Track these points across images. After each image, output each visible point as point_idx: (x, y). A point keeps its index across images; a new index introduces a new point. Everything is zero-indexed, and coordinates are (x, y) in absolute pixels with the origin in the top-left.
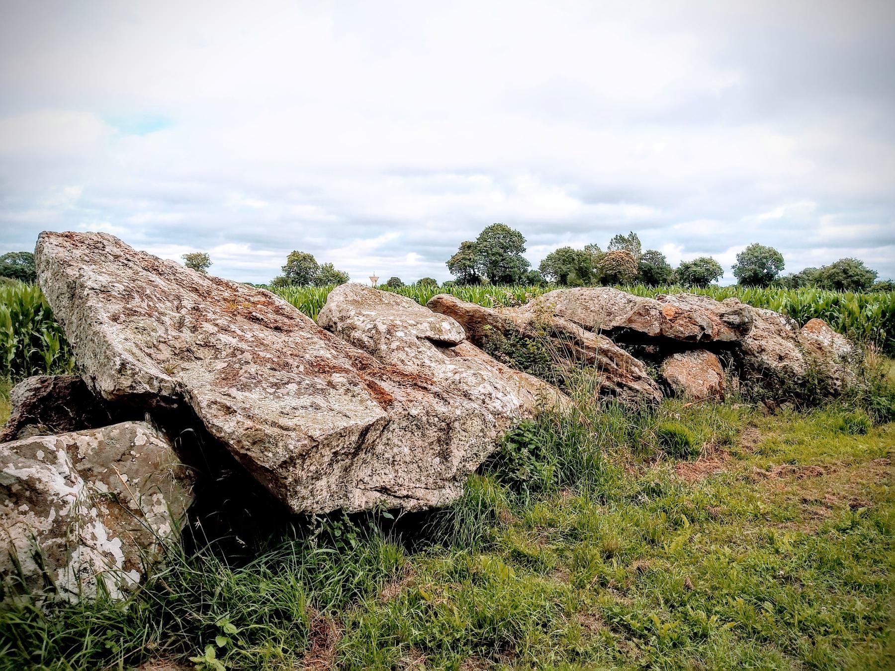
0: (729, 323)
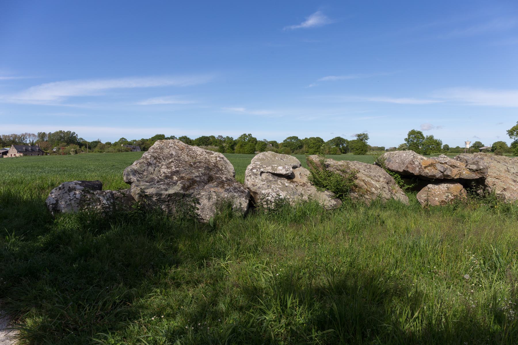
0: (470, 169)
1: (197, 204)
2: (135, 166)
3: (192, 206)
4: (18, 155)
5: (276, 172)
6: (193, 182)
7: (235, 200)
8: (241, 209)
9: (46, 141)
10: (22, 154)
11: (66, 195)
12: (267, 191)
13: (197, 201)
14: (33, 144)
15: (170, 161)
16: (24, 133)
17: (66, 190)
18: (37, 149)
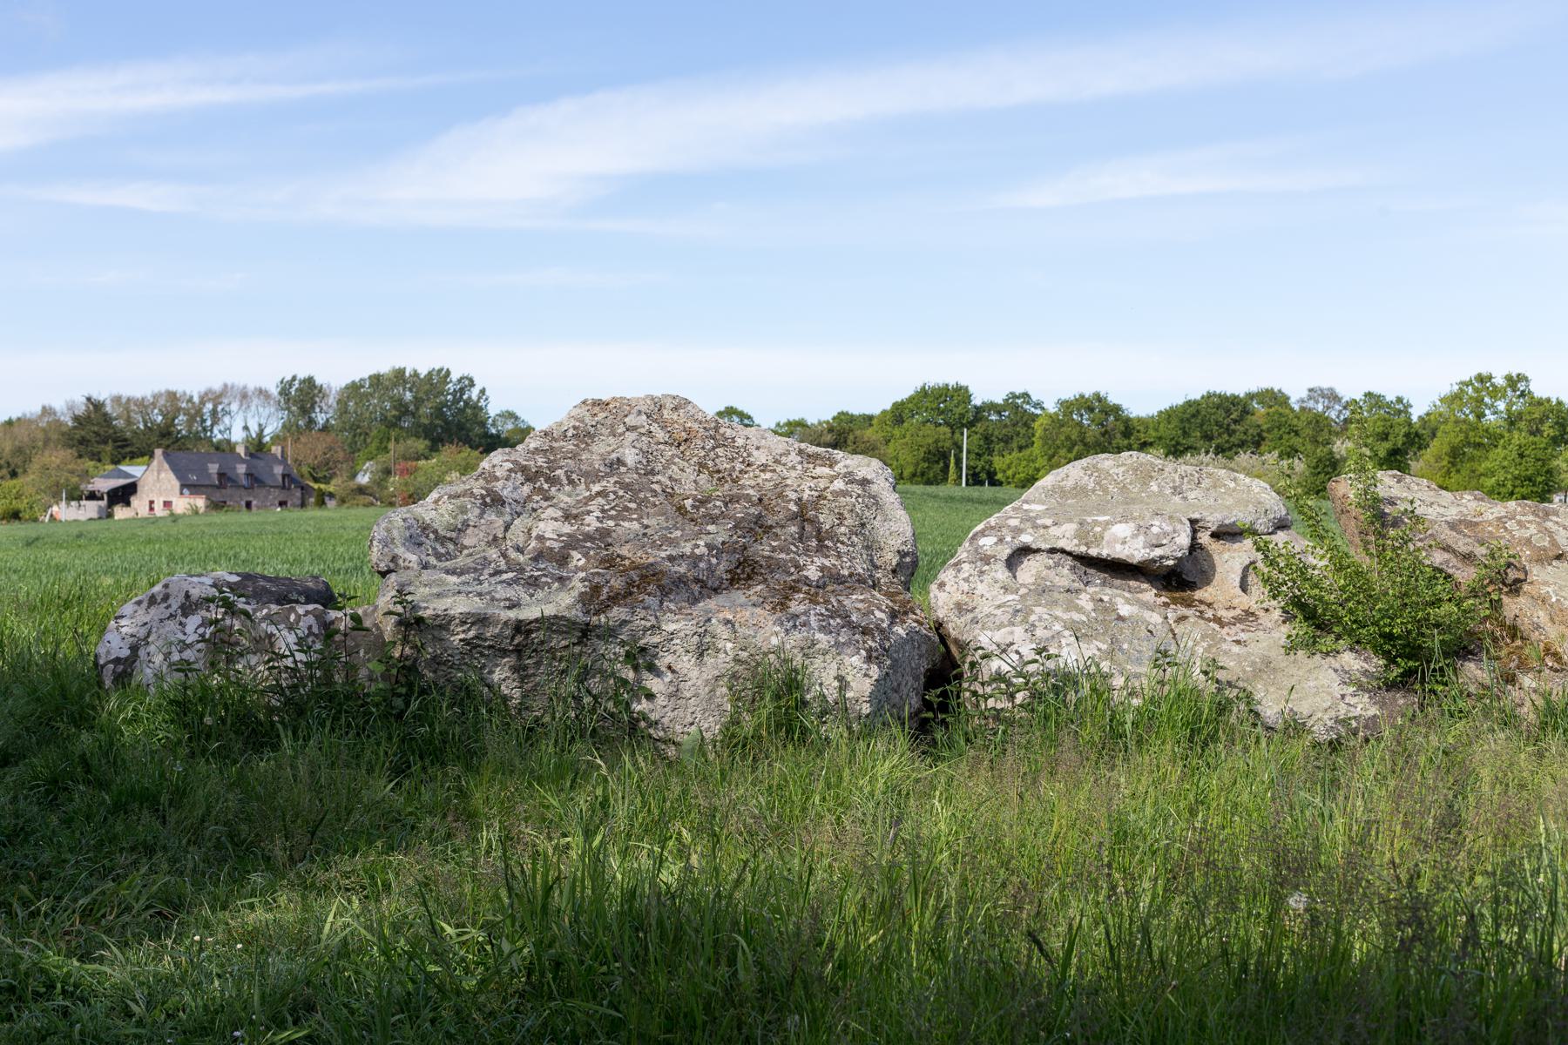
1: (646, 675)
2: (435, 509)
3: (625, 682)
4: (182, 504)
5: (1093, 552)
6: (650, 582)
7: (818, 662)
8: (842, 707)
9: (326, 428)
10: (200, 502)
11: (172, 625)
12: (1001, 636)
13: (642, 658)
14: (257, 448)
15: (596, 488)
16: (217, 386)
17: (175, 606)
18: (278, 470)
